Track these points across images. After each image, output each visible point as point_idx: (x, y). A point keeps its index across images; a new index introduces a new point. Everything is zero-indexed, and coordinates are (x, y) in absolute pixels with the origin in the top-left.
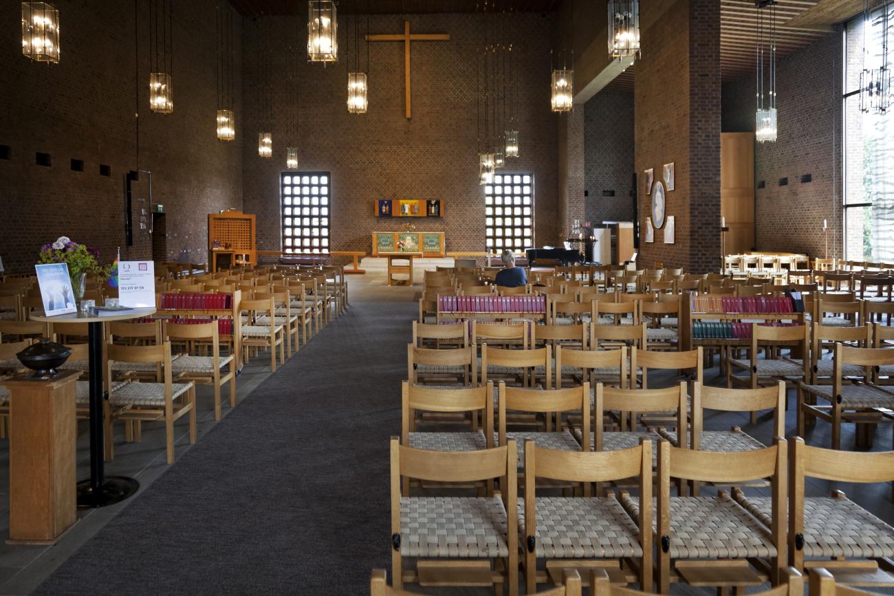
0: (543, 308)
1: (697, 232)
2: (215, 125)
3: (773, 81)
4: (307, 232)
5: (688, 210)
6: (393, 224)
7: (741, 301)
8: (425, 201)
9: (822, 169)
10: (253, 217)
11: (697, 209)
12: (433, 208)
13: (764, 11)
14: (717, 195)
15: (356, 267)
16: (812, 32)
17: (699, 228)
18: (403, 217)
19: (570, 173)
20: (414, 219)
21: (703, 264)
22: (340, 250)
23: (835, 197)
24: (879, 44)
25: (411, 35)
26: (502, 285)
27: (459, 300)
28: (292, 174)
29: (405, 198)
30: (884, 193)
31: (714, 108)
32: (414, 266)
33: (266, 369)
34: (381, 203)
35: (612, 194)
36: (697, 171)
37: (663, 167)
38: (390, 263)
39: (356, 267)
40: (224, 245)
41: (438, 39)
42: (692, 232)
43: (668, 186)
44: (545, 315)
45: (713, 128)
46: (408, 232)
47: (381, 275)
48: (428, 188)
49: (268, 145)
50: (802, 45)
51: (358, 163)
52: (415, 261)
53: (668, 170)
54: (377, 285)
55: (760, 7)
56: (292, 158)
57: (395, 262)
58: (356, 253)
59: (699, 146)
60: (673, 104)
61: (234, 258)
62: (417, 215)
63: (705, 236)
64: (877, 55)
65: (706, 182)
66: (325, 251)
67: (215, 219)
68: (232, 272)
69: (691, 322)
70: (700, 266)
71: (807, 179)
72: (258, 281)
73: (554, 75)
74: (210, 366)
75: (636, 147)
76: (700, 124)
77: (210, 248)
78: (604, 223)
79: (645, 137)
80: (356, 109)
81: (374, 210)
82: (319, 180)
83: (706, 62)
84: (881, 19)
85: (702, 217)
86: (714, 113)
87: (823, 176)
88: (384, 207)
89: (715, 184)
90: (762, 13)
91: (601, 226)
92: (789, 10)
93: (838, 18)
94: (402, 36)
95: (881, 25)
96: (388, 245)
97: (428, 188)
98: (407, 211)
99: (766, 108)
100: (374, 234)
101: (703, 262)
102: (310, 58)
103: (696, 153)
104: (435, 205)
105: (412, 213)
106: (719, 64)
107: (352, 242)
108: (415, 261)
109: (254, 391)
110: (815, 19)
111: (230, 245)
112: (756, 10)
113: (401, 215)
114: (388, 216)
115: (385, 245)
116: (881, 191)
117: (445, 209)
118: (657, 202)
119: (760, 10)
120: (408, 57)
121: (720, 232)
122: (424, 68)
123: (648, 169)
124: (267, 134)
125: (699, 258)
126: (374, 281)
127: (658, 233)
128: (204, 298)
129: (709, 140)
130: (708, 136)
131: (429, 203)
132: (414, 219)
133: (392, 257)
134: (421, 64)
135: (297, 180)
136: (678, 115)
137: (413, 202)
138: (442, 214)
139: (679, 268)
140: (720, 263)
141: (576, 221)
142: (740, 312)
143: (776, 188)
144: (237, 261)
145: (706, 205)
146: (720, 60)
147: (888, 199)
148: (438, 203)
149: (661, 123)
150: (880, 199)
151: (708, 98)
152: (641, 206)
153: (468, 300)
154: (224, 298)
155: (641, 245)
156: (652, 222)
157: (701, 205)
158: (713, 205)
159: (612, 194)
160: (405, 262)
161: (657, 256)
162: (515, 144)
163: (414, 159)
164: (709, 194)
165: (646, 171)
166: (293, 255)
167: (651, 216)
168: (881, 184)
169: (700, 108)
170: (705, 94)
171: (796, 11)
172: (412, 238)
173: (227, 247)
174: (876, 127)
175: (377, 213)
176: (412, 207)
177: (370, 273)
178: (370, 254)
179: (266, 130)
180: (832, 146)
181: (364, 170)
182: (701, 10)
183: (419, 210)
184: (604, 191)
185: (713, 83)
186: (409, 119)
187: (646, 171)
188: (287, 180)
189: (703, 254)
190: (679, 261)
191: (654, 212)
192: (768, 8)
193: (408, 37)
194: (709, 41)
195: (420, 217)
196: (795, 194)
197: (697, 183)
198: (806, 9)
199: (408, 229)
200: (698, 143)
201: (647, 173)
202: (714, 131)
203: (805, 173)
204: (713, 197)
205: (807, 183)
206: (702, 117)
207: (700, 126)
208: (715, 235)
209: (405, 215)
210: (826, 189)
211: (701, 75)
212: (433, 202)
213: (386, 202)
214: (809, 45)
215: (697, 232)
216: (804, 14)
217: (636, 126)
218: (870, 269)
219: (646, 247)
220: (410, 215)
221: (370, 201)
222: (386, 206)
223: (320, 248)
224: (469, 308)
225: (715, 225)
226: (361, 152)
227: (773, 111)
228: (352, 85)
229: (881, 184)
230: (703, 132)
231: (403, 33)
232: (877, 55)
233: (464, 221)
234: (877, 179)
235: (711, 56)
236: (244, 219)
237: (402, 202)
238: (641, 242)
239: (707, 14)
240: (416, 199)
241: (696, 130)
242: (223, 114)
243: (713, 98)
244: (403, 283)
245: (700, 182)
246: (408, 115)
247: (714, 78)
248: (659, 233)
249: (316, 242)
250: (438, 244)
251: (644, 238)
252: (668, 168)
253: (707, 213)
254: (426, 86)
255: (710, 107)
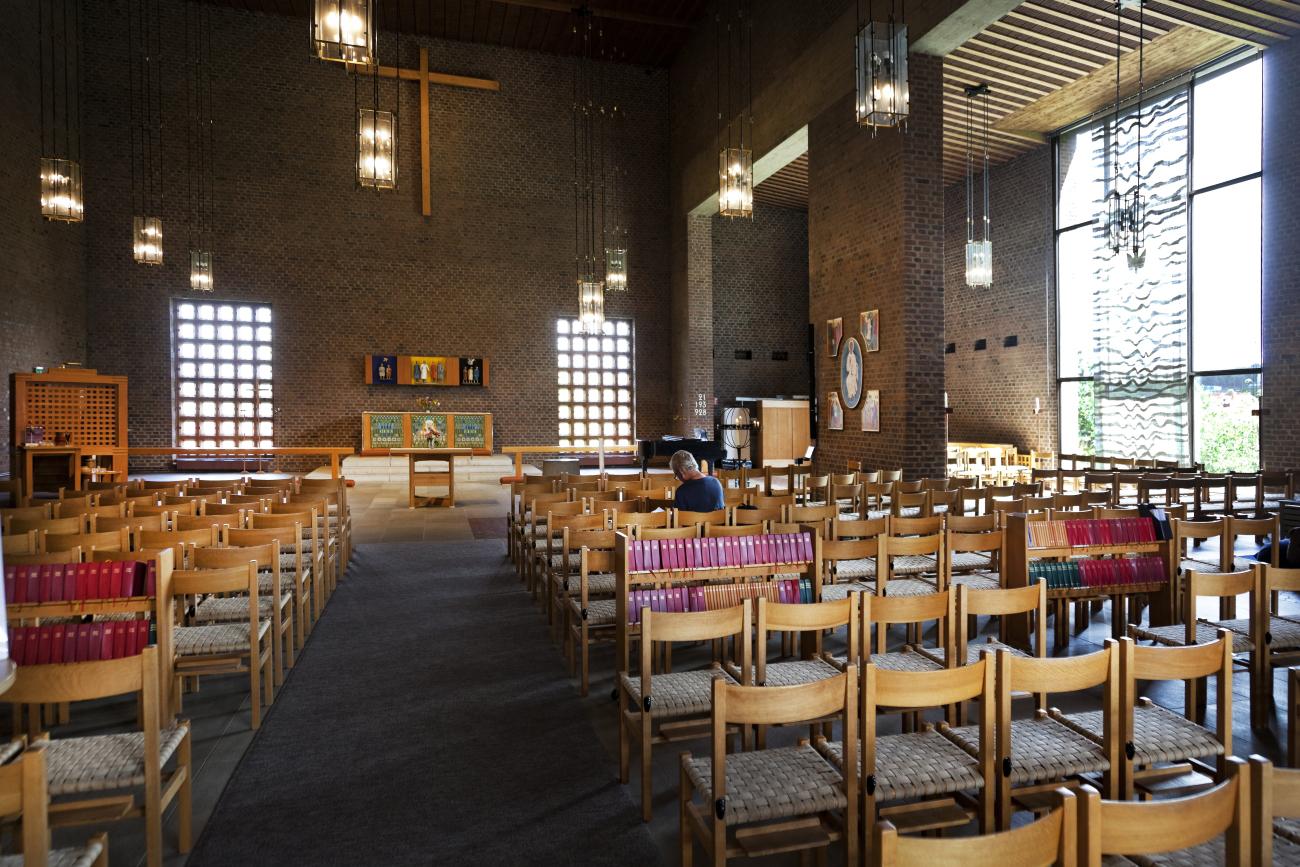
0: (809, 553)
1: (916, 414)
2: (37, 189)
3: (987, 205)
4: (228, 409)
5: (901, 382)
6: (398, 398)
7: (1090, 526)
8: (456, 362)
9: (1030, 330)
10: (123, 382)
11: (914, 380)
12: (471, 371)
13: (974, 102)
14: (940, 360)
15: (335, 474)
16: (1021, 141)
17: (918, 409)
18: (416, 386)
19: (692, 322)
20: (436, 389)
21: (923, 463)
22: (297, 444)
23: (1049, 367)
24: (1100, 166)
25: (431, 74)
26: (688, 509)
27: (664, 547)
28: (199, 297)
29: (420, 354)
30: (1109, 364)
31: (936, 231)
32: (456, 470)
33: (233, 724)
34: (377, 362)
35: (748, 355)
36: (915, 323)
37: (859, 315)
38: (412, 467)
39: (335, 474)
40: (53, 436)
41: (464, 84)
42: (909, 414)
43: (867, 344)
44: (812, 567)
45: (935, 261)
46: (428, 412)
47: (384, 487)
48: (461, 337)
49: (153, 241)
50: (1004, 157)
51: (331, 289)
52: (457, 461)
53: (868, 321)
54: (388, 509)
55: (969, 96)
56: (200, 270)
57: (422, 466)
58: (334, 451)
59: (917, 286)
60: (875, 221)
61: (78, 462)
62: (442, 383)
63: (926, 420)
64: (1099, 180)
65: (926, 340)
66: (267, 445)
67: (29, 383)
68: (98, 497)
69: (1027, 565)
70: (919, 465)
71: (1011, 342)
72: (136, 506)
73: (723, 155)
74: (131, 767)
75: (810, 284)
76: (918, 253)
77: (18, 443)
78: (738, 399)
79: (827, 270)
80: (375, 180)
81: (363, 373)
82: (235, 313)
83: (925, 162)
84: (1102, 133)
85: (921, 392)
86: (935, 239)
87: (1032, 338)
88: (382, 368)
89: (937, 344)
90: (971, 105)
91: (734, 404)
92: (1002, 105)
93: (1053, 125)
94: (415, 72)
95: (1102, 140)
96: (392, 435)
97: (461, 337)
98: (424, 375)
99: (978, 238)
100: (366, 416)
101: (922, 459)
102: (315, 52)
103: (913, 296)
104: (474, 366)
105: (434, 379)
106: (942, 166)
107: (322, 429)
108: (457, 461)
109: (227, 795)
110: (1028, 123)
111: (68, 437)
112: (965, 99)
113: (413, 382)
114: (391, 383)
115: (384, 435)
116: (1106, 362)
117: (492, 374)
118: (848, 369)
119: (970, 101)
120: (425, 110)
121: (944, 414)
122: (454, 134)
123: (834, 318)
124: (153, 220)
125: (918, 454)
126: (378, 501)
127: (852, 415)
128: (70, 573)
129: (929, 278)
130: (928, 272)
131: (463, 364)
132: (436, 389)
133: (417, 457)
134: (449, 125)
135: (206, 312)
136: (884, 238)
137: (436, 360)
138: (486, 382)
139: (896, 470)
140: (941, 459)
141: (700, 396)
142: (1089, 543)
143: (971, 354)
144: (86, 469)
145: (927, 375)
146: (942, 161)
147: (1114, 372)
148: (479, 363)
149: (855, 249)
150: (1104, 372)
151: (927, 216)
152: (822, 374)
153: (681, 546)
154: (129, 570)
155: (820, 434)
156: (841, 399)
157: (919, 374)
158: (935, 375)
159: (748, 355)
160: (441, 466)
161: (850, 451)
162: (621, 270)
163: (437, 287)
164: (930, 358)
165: (830, 321)
166: (218, 453)
167: (838, 389)
168: (1105, 351)
169: (917, 230)
170: (924, 209)
171: (1009, 107)
172: (435, 422)
173: (58, 440)
174: (1098, 275)
175: (369, 378)
176: (433, 370)
177: (363, 485)
178: (358, 453)
179: (149, 213)
180: (1045, 298)
181: (344, 301)
182: (919, 84)
183: (445, 376)
184: (737, 352)
185: (934, 194)
186: (427, 217)
187: (830, 321)
188: (186, 311)
189: (924, 448)
190: (887, 458)
191: (845, 383)
192: (978, 99)
193: (425, 77)
194: (928, 131)
195: (448, 387)
196: (996, 362)
197: (914, 342)
198: (1000, 117)
199: (426, 406)
200: (916, 282)
201: (831, 324)
202: (936, 265)
203: (1009, 334)
204: (934, 363)
205: (1012, 348)
206: (920, 243)
207: (918, 256)
208: (938, 420)
209: (421, 382)
210: (1037, 356)
211: (919, 181)
212: (471, 362)
213: (386, 359)
214: (1013, 158)
215: (916, 414)
216: (1018, 113)
217: (811, 253)
218: (1098, 466)
219: (830, 437)
220: (429, 382)
221: (356, 356)
222: (386, 367)
223: (256, 438)
224: (682, 563)
225: (937, 405)
226: (339, 269)
227: (988, 244)
228: (367, 134)
229: (1105, 351)
230: (922, 266)
231: (416, 67)
232: (1099, 180)
233: (522, 395)
234: (1099, 344)
235: (931, 154)
236: (101, 385)
237: (414, 359)
238: (821, 429)
239: (926, 91)
240: (441, 356)
241: (913, 262)
242: (56, 169)
243: (934, 216)
244: (438, 502)
245: (918, 340)
246: (427, 210)
247: (936, 186)
248: (852, 415)
249: (247, 429)
250: (481, 432)
251: (826, 424)
252: (869, 317)
253: (928, 386)
254: (458, 165)
255: (931, 229)
